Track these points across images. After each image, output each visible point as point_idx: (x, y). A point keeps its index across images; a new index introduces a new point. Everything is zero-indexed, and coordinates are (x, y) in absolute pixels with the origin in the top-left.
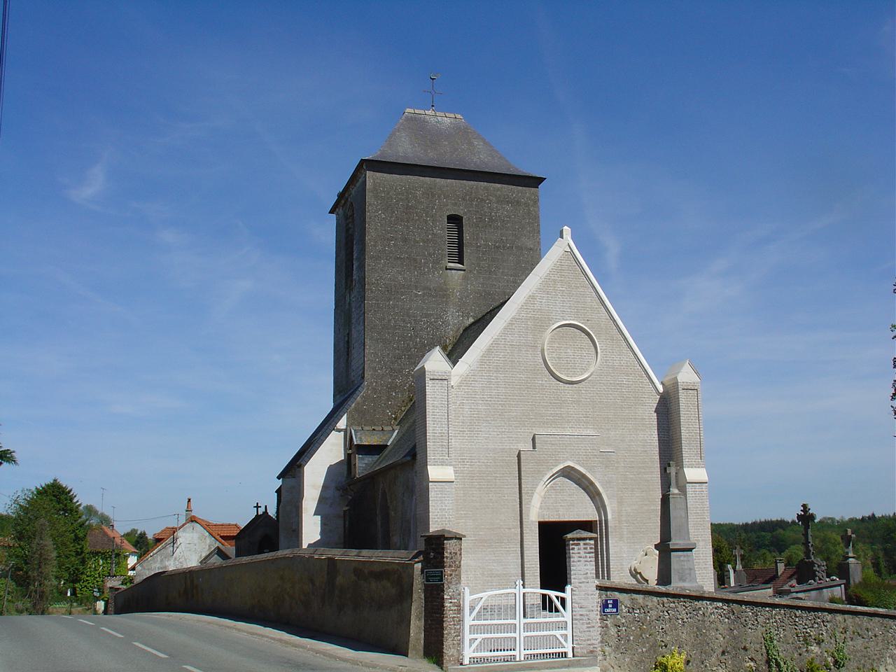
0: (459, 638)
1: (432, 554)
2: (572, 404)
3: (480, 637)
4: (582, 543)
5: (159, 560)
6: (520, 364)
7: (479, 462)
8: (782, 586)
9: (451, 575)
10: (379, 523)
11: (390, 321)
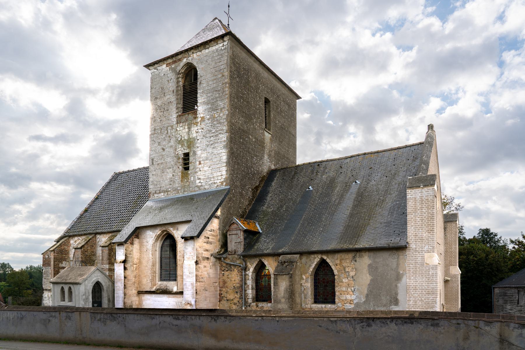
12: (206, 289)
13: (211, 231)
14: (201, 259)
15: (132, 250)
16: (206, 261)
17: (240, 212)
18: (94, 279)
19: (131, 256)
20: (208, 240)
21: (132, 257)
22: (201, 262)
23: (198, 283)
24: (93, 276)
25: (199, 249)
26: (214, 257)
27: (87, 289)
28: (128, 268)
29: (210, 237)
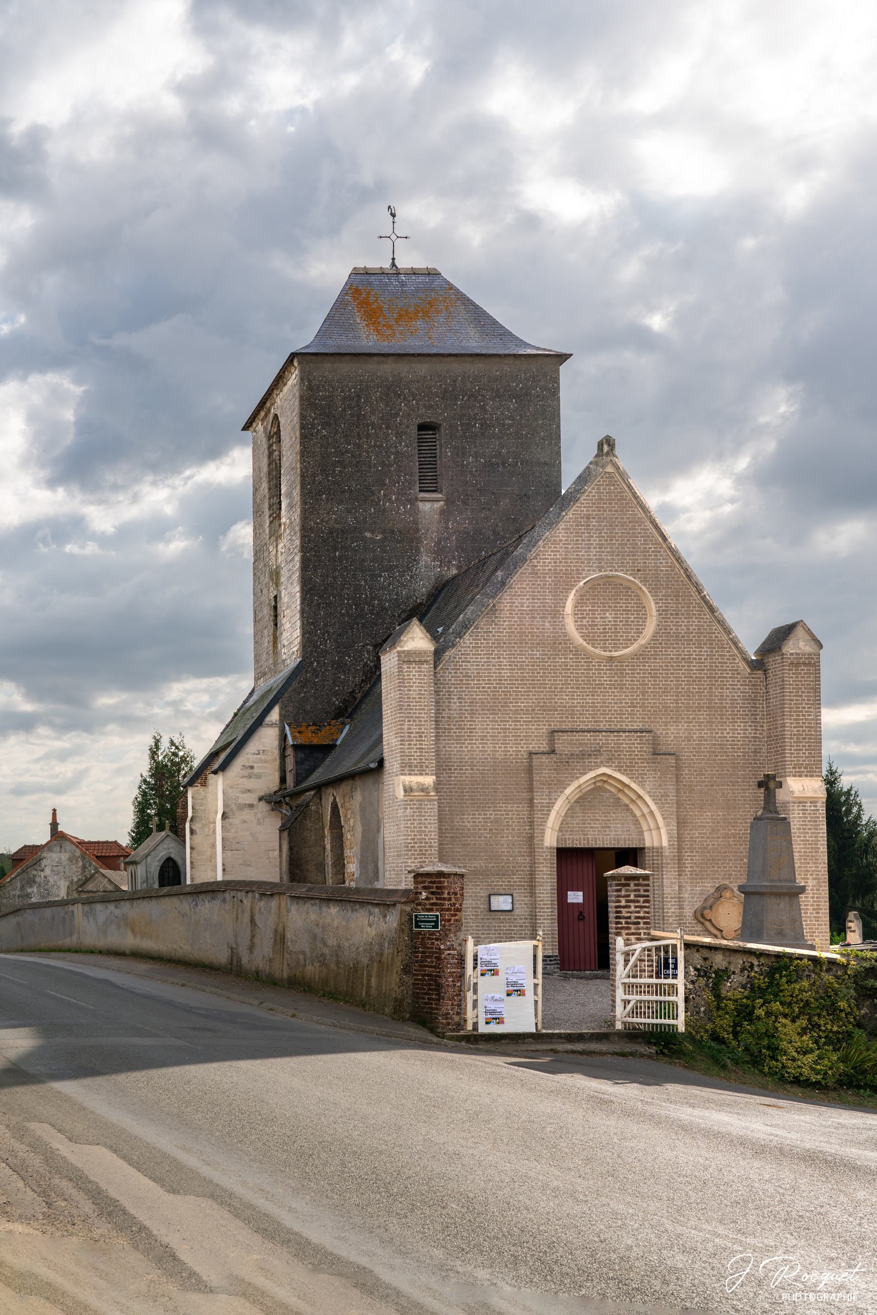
0: (459, 997)
1: (424, 894)
2: (610, 688)
3: (634, 998)
4: (632, 883)
5: (19, 886)
6: (532, 636)
7: (472, 769)
8: (443, 629)
9: (449, 920)
10: (328, 847)
11: (335, 578)
12: (248, 863)
13: (259, 754)
14: (235, 809)
15: (205, 797)
16: (247, 811)
17: (337, 703)
18: (162, 854)
19: (203, 808)
20: (251, 771)
21: (205, 810)
22: (233, 814)
23: (229, 853)
24: (160, 847)
25: (230, 791)
26: (267, 802)
27: (150, 873)
28: (198, 831)
29: (256, 765)
